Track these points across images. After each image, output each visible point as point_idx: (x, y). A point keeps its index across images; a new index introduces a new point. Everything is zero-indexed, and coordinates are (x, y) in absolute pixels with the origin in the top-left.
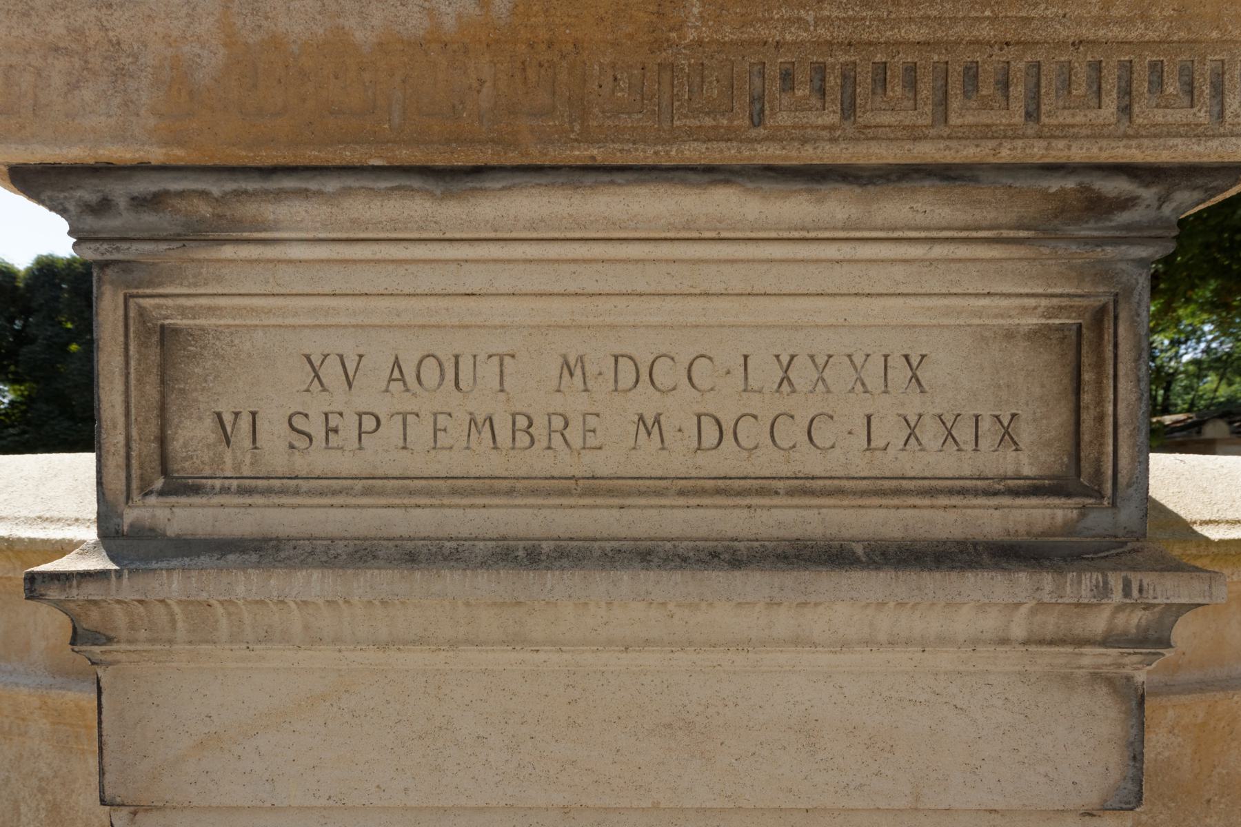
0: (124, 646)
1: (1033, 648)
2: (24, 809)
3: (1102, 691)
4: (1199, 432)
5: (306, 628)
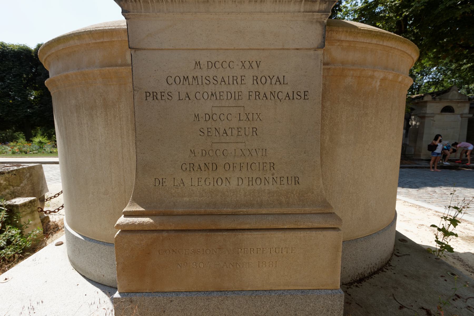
0: (132, 13)
1: (305, 13)
2: (97, 101)
3: (318, 24)
4: (422, 99)
5: (167, 9)
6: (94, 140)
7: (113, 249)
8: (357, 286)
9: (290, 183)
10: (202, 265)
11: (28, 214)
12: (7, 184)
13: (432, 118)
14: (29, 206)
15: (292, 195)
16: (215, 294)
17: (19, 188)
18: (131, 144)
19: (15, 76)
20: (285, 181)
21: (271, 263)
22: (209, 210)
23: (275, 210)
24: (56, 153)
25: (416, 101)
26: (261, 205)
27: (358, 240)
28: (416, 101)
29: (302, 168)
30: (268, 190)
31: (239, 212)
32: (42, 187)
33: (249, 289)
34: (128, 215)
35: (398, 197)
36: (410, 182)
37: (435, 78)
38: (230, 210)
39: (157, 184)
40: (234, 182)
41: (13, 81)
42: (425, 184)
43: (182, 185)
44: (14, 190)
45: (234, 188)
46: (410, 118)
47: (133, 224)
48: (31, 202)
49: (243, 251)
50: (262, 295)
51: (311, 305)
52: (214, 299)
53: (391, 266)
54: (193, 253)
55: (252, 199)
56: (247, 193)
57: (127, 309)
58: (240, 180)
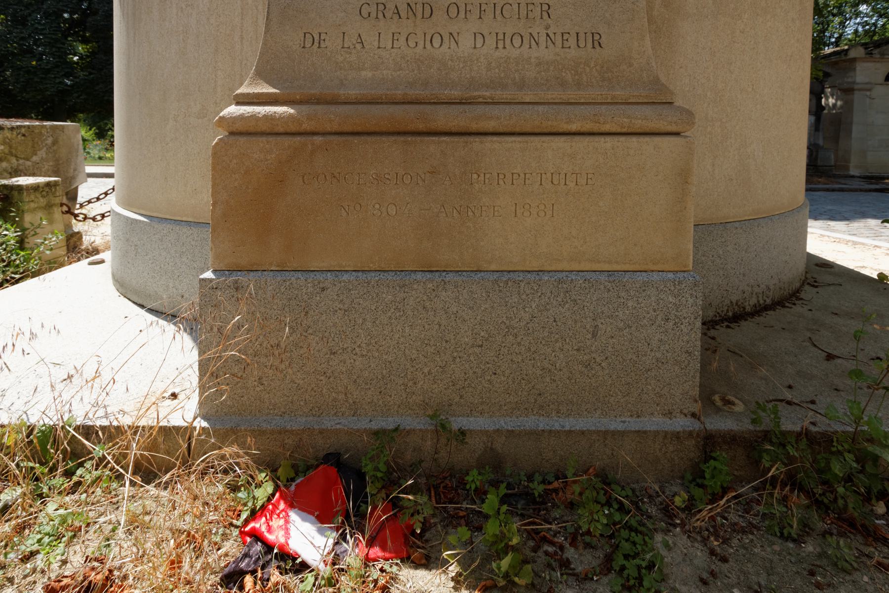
4: (846, 55)
6: (187, 6)
7: (207, 233)
8: (728, 327)
9: (582, 45)
10: (392, 210)
11: (40, 208)
12: (7, 151)
13: (868, 93)
14: (44, 193)
15: (588, 69)
16: (419, 276)
17: (28, 163)
18: (260, 7)
19: (46, 15)
20: (572, 41)
21: (543, 207)
22: (413, 93)
23: (551, 95)
24: (112, 159)
25: (833, 59)
26: (522, 85)
27: (729, 225)
28: (833, 59)
29: (607, 15)
30: (537, 58)
31: (475, 98)
32: (75, 170)
33: (493, 267)
34: (243, 100)
35: (809, 230)
36: (830, 210)
37: (867, 23)
38: (456, 93)
39: (308, 45)
40: (466, 42)
41: (44, 24)
42: (864, 215)
43: (359, 46)
44: (19, 165)
45: (466, 54)
46: (823, 92)
47: (253, 117)
48: (48, 184)
49: (482, 178)
50: (521, 279)
51: (630, 304)
52: (415, 286)
53: (802, 299)
54: (376, 182)
55: (502, 75)
56: (493, 64)
57: (228, 384)
58: (479, 37)
